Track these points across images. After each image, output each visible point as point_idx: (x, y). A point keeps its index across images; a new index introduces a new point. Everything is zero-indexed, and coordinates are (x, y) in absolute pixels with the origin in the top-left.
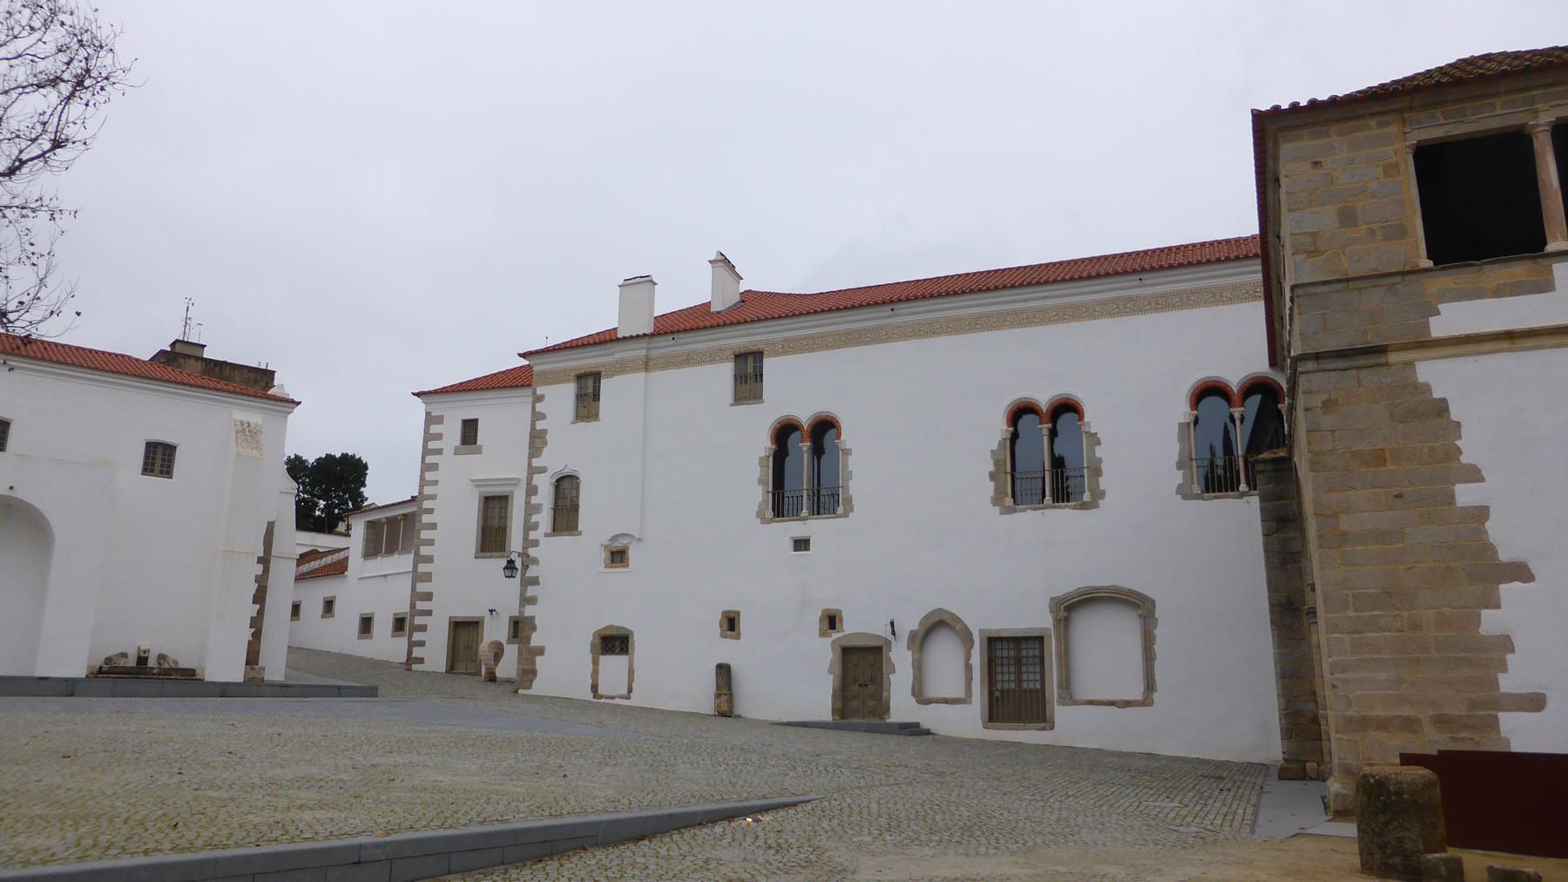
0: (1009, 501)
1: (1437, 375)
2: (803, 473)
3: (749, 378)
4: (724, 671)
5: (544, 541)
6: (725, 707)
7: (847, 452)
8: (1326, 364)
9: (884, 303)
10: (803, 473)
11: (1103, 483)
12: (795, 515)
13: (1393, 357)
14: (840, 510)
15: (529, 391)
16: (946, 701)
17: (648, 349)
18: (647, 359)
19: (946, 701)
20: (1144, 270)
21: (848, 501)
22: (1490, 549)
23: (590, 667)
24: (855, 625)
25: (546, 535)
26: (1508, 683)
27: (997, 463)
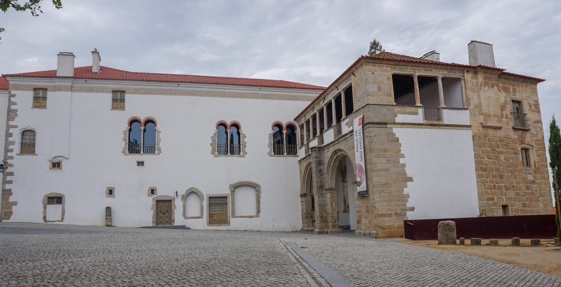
0: (216, 153)
1: (398, 131)
2: (141, 138)
3: (118, 101)
4: (108, 209)
5: (16, 157)
6: (109, 223)
7: (160, 132)
8: (375, 126)
9: (176, 82)
10: (141, 138)
11: (246, 150)
12: (138, 152)
13: (388, 126)
14: (156, 152)
15: (7, 92)
16: (194, 218)
17: (72, 83)
18: (72, 87)
19: (194, 218)
20: (262, 86)
21: (159, 150)
22: (405, 174)
23: (43, 210)
24: (161, 193)
25: (18, 154)
26: (409, 205)
27: (213, 140)
